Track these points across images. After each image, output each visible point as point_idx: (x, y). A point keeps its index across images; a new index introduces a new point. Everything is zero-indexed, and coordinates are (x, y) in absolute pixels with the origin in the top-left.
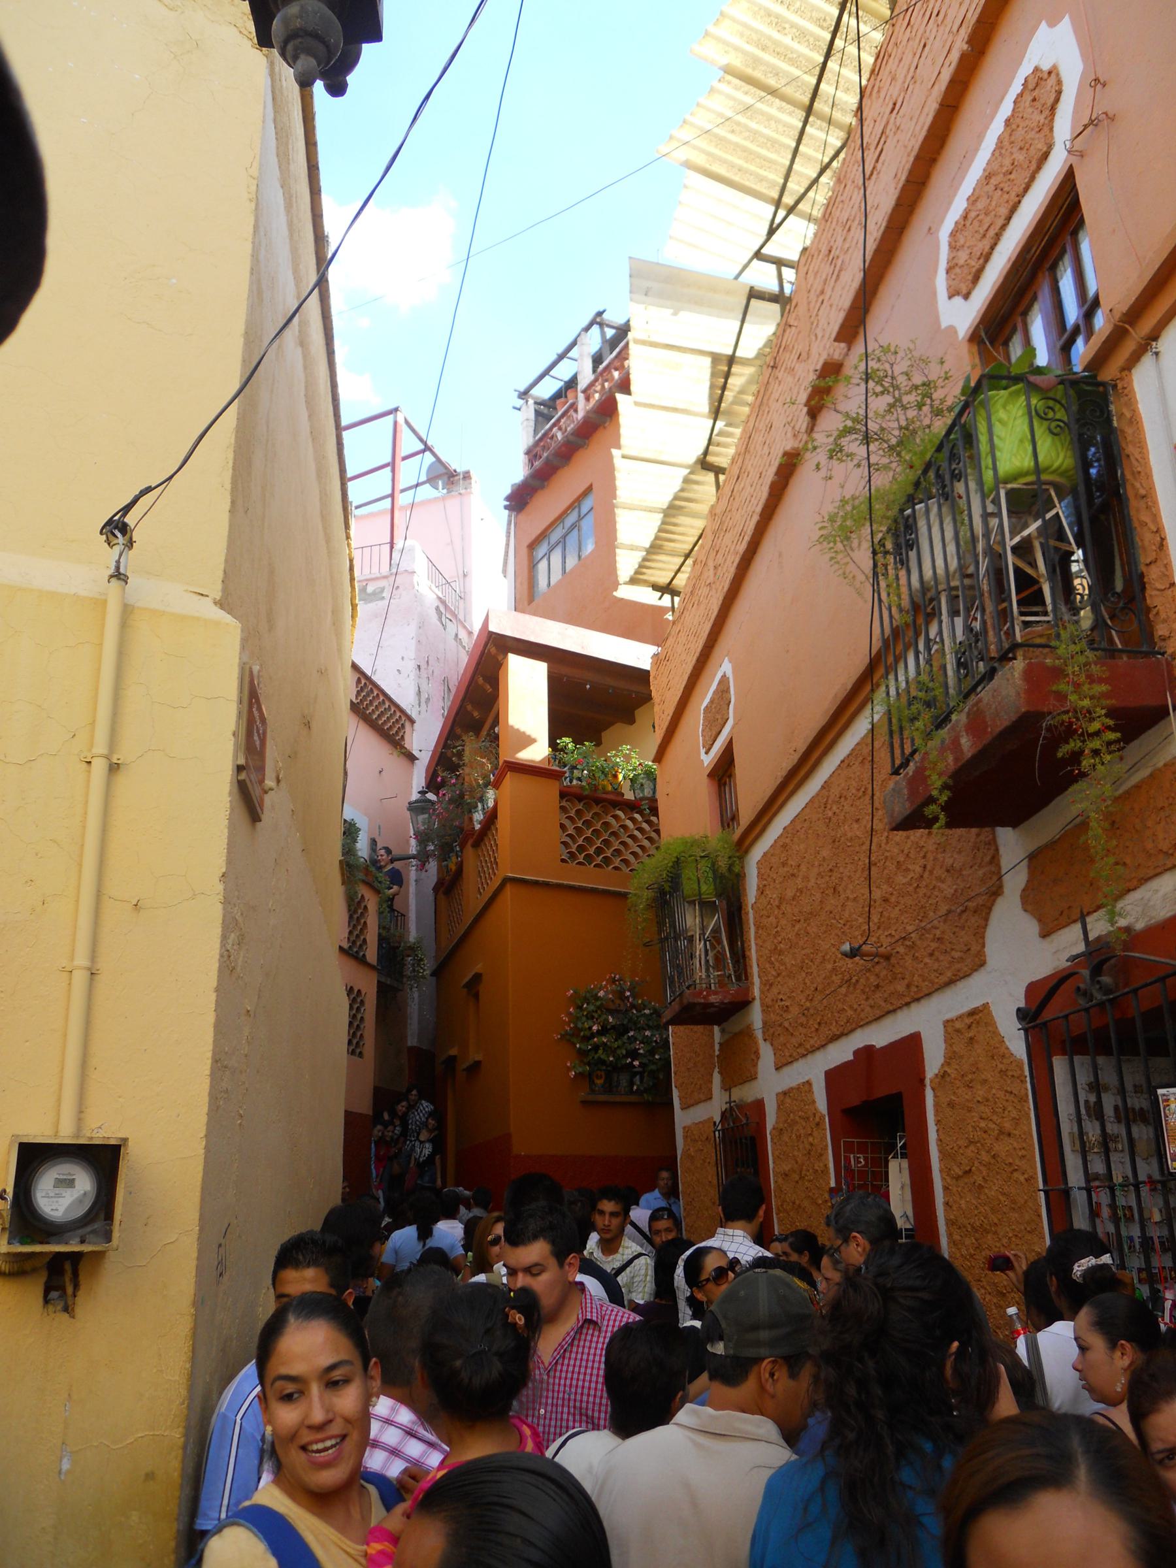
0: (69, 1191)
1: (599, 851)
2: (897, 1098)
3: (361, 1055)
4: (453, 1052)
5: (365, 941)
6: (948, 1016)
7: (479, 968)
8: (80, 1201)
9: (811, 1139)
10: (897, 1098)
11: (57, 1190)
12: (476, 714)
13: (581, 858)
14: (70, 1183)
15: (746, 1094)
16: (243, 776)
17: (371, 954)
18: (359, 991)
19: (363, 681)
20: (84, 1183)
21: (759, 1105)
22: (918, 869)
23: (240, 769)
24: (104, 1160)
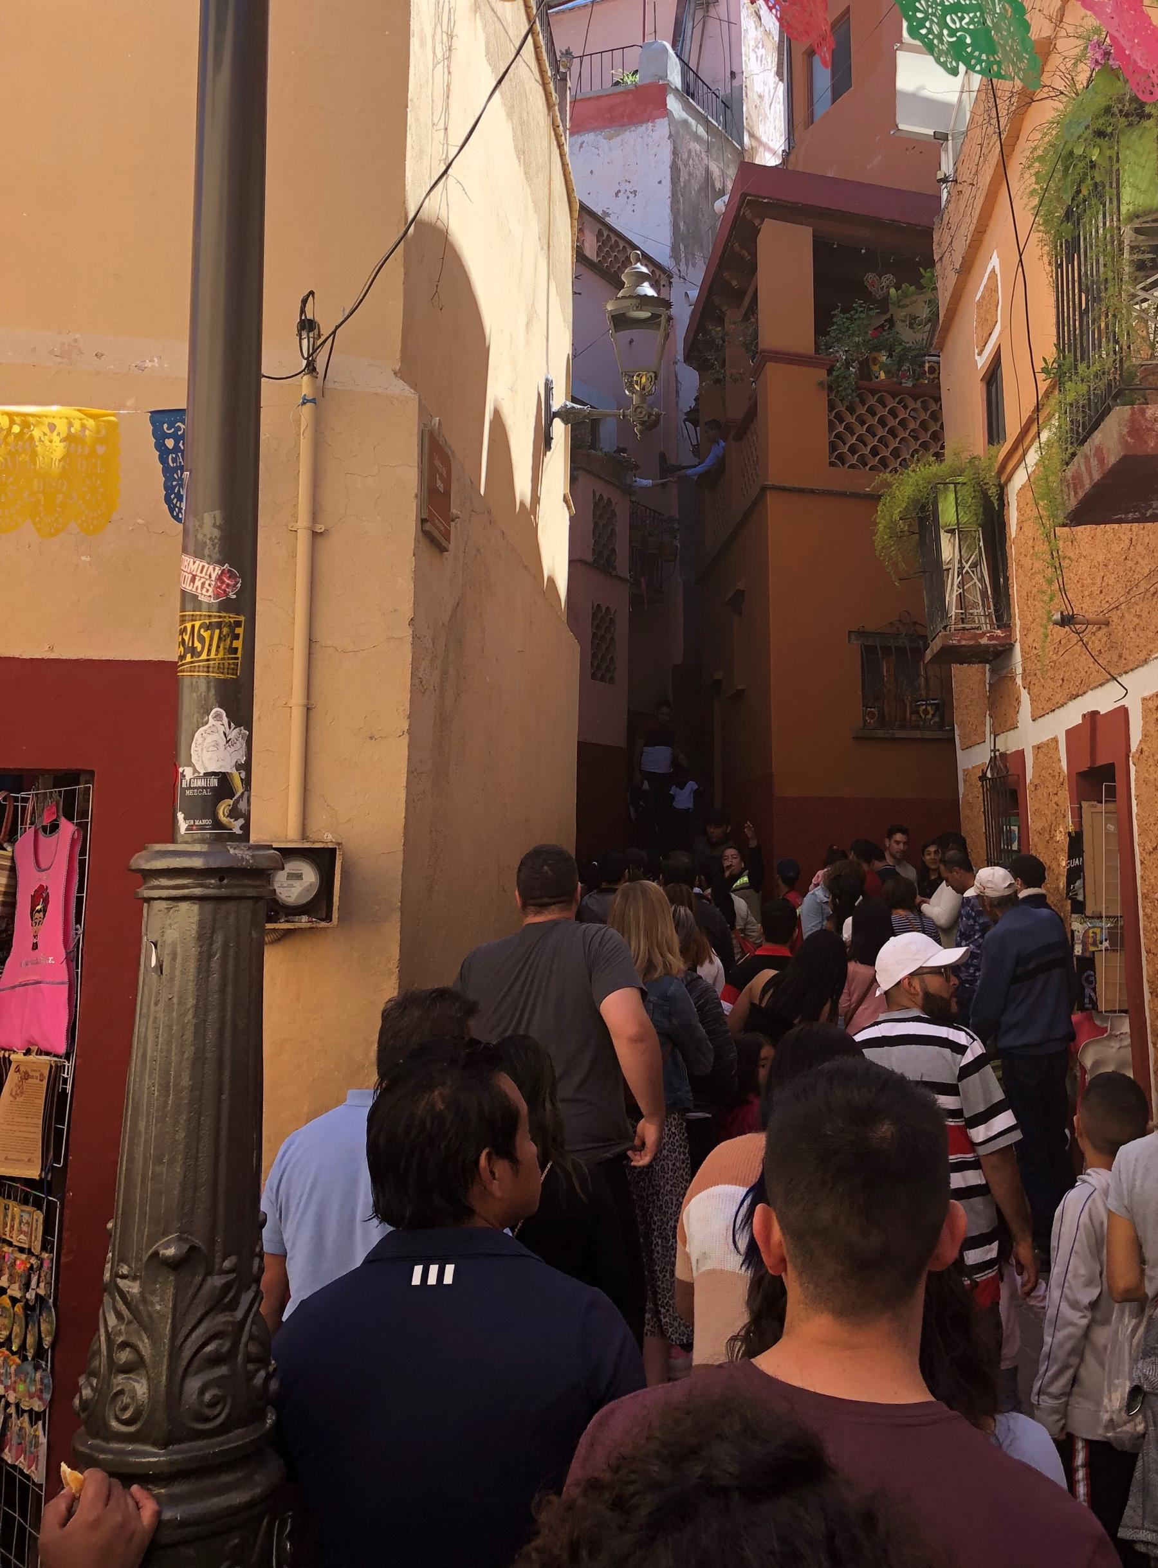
0: (298, 882)
1: (874, 452)
2: (1112, 766)
3: (612, 680)
4: (718, 675)
5: (613, 551)
6: (1147, 694)
7: (741, 585)
8: (307, 890)
9: (1056, 798)
10: (1112, 766)
11: (290, 882)
12: (734, 283)
13: (854, 460)
14: (299, 876)
15: (1009, 743)
16: (428, 527)
17: (622, 565)
18: (608, 608)
19: (605, 233)
20: (310, 876)
21: (1021, 754)
22: (1128, 541)
23: (423, 521)
24: (323, 859)
